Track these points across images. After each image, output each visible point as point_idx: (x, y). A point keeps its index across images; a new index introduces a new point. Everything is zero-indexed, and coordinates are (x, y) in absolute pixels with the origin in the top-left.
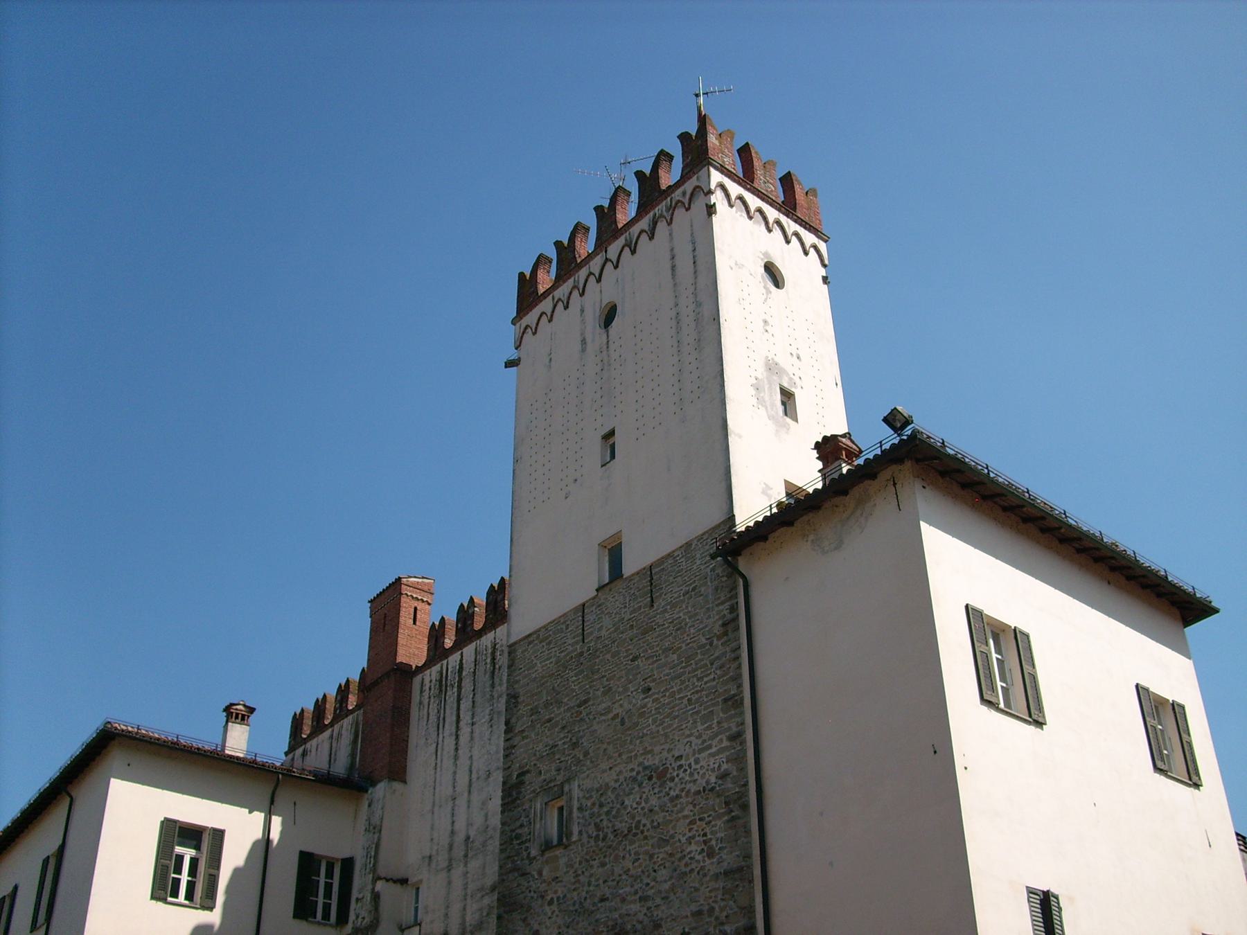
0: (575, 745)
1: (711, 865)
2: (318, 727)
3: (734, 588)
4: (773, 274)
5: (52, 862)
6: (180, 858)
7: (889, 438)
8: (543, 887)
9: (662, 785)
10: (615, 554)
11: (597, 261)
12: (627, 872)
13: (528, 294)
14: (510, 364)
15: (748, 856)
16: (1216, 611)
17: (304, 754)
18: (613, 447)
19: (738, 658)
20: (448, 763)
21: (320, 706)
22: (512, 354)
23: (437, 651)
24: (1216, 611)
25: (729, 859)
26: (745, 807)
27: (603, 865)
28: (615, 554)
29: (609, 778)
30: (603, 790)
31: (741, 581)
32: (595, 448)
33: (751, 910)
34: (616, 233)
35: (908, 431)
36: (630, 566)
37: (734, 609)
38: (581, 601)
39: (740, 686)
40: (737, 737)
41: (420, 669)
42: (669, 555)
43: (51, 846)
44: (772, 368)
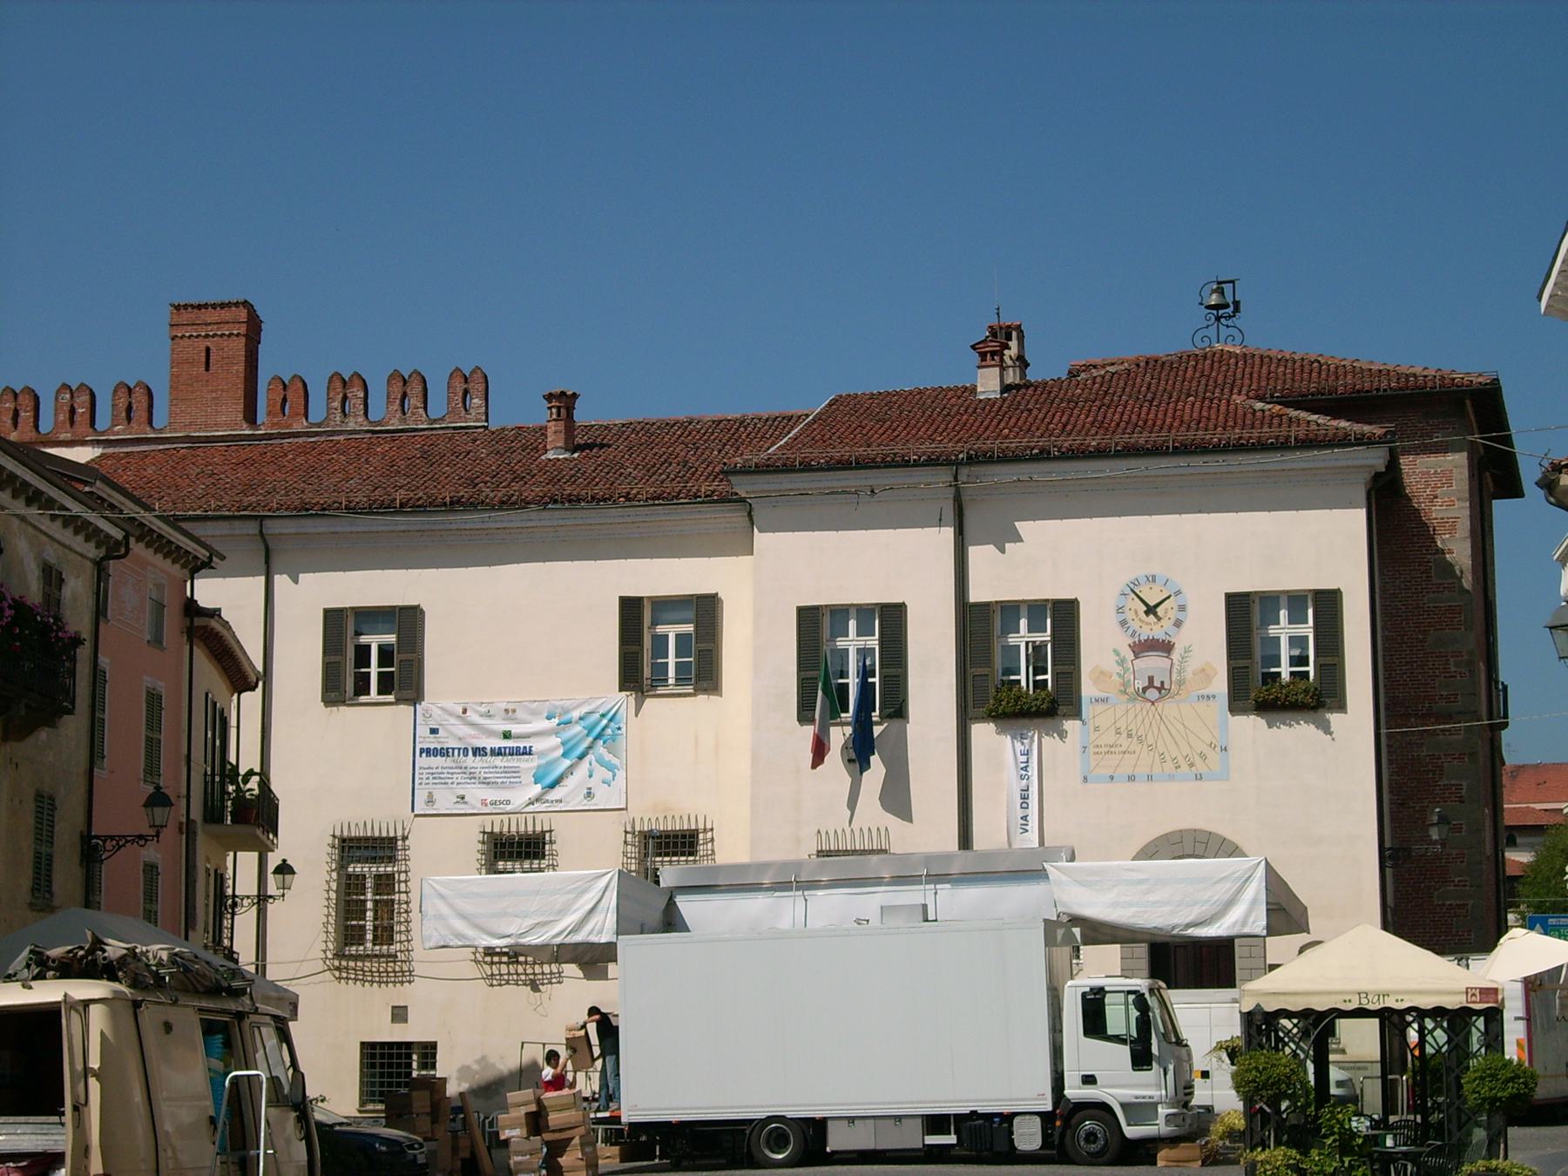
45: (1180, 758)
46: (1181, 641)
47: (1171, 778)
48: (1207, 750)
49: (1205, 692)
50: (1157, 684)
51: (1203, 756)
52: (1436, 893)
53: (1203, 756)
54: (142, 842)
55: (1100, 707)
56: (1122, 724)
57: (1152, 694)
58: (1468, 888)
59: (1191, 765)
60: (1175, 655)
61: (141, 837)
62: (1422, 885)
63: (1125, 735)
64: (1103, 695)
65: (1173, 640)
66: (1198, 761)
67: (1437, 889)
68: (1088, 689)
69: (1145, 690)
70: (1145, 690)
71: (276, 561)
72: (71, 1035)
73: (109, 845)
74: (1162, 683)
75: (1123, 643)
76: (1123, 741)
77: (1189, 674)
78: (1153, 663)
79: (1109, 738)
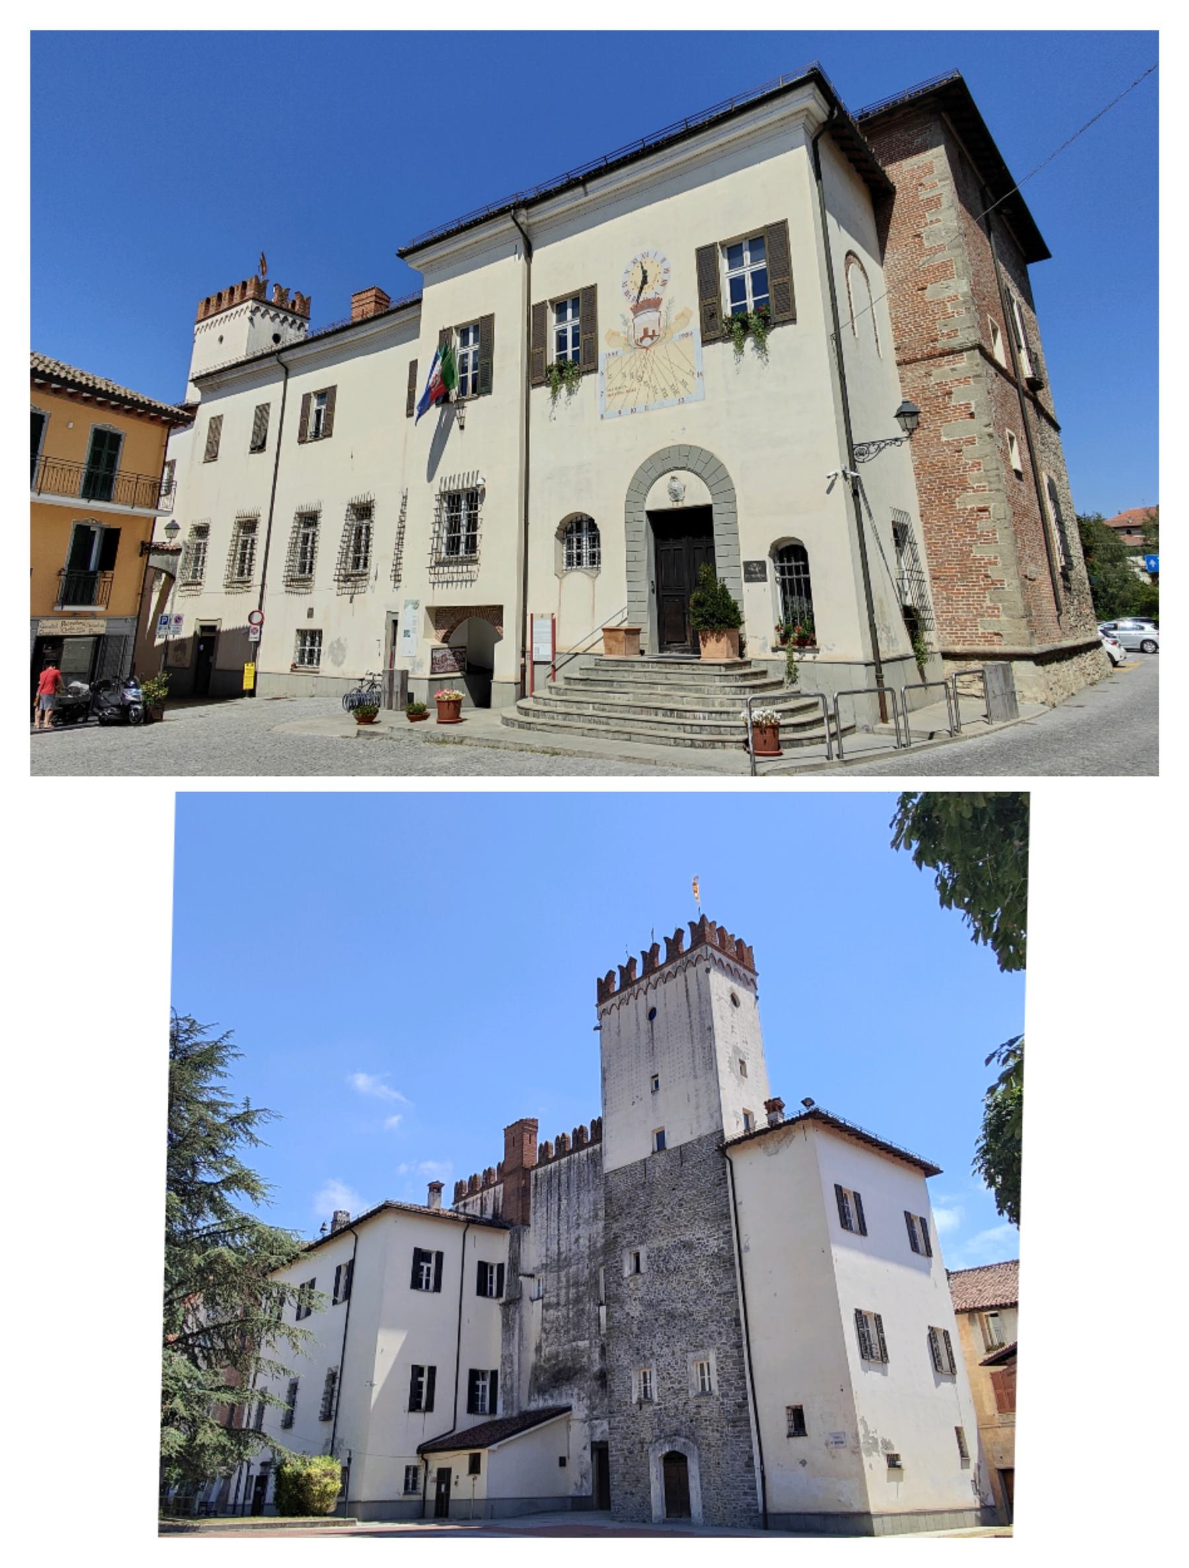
0: (644, 1226)
1: (717, 1290)
2: (472, 1192)
3: (724, 1164)
4: (735, 1001)
5: (344, 1271)
6: (423, 1267)
7: (804, 1110)
8: (630, 1292)
9: (691, 1251)
10: (660, 1137)
11: (644, 983)
12: (674, 1289)
13: (604, 991)
14: (596, 1029)
15: (736, 1287)
16: (942, 1172)
17: (465, 1205)
18: (657, 1083)
19: (727, 1196)
20: (554, 1218)
21: (473, 1179)
22: (597, 1023)
23: (545, 1158)
24: (942, 1172)
25: (727, 1287)
26: (733, 1265)
27: (662, 1284)
28: (660, 1137)
29: (664, 1244)
30: (660, 1250)
31: (728, 1162)
32: (648, 1086)
33: (738, 1311)
34: (655, 970)
35: (813, 1107)
36: (671, 1144)
37: (724, 1173)
38: (643, 1157)
39: (729, 1209)
40: (728, 1232)
41: (533, 1168)
42: (690, 1143)
43: (345, 1260)
44: (736, 1050)
45: (668, 389)
46: (666, 295)
47: (662, 406)
48: (688, 379)
49: (684, 331)
50: (650, 333)
51: (684, 383)
52: (957, 499)
53: (684, 383)
54: (899, 443)
55: (612, 360)
56: (627, 370)
57: (647, 342)
58: (987, 492)
59: (676, 392)
60: (662, 308)
61: (896, 440)
62: (944, 493)
63: (628, 378)
64: (615, 351)
65: (660, 296)
66: (680, 387)
67: (958, 496)
68: (603, 348)
69: (642, 339)
70: (642, 339)
71: (290, 373)
72: (1070, 658)
73: (872, 449)
74: (654, 331)
75: (627, 305)
76: (628, 382)
77: (672, 319)
78: (648, 319)
79: (618, 382)
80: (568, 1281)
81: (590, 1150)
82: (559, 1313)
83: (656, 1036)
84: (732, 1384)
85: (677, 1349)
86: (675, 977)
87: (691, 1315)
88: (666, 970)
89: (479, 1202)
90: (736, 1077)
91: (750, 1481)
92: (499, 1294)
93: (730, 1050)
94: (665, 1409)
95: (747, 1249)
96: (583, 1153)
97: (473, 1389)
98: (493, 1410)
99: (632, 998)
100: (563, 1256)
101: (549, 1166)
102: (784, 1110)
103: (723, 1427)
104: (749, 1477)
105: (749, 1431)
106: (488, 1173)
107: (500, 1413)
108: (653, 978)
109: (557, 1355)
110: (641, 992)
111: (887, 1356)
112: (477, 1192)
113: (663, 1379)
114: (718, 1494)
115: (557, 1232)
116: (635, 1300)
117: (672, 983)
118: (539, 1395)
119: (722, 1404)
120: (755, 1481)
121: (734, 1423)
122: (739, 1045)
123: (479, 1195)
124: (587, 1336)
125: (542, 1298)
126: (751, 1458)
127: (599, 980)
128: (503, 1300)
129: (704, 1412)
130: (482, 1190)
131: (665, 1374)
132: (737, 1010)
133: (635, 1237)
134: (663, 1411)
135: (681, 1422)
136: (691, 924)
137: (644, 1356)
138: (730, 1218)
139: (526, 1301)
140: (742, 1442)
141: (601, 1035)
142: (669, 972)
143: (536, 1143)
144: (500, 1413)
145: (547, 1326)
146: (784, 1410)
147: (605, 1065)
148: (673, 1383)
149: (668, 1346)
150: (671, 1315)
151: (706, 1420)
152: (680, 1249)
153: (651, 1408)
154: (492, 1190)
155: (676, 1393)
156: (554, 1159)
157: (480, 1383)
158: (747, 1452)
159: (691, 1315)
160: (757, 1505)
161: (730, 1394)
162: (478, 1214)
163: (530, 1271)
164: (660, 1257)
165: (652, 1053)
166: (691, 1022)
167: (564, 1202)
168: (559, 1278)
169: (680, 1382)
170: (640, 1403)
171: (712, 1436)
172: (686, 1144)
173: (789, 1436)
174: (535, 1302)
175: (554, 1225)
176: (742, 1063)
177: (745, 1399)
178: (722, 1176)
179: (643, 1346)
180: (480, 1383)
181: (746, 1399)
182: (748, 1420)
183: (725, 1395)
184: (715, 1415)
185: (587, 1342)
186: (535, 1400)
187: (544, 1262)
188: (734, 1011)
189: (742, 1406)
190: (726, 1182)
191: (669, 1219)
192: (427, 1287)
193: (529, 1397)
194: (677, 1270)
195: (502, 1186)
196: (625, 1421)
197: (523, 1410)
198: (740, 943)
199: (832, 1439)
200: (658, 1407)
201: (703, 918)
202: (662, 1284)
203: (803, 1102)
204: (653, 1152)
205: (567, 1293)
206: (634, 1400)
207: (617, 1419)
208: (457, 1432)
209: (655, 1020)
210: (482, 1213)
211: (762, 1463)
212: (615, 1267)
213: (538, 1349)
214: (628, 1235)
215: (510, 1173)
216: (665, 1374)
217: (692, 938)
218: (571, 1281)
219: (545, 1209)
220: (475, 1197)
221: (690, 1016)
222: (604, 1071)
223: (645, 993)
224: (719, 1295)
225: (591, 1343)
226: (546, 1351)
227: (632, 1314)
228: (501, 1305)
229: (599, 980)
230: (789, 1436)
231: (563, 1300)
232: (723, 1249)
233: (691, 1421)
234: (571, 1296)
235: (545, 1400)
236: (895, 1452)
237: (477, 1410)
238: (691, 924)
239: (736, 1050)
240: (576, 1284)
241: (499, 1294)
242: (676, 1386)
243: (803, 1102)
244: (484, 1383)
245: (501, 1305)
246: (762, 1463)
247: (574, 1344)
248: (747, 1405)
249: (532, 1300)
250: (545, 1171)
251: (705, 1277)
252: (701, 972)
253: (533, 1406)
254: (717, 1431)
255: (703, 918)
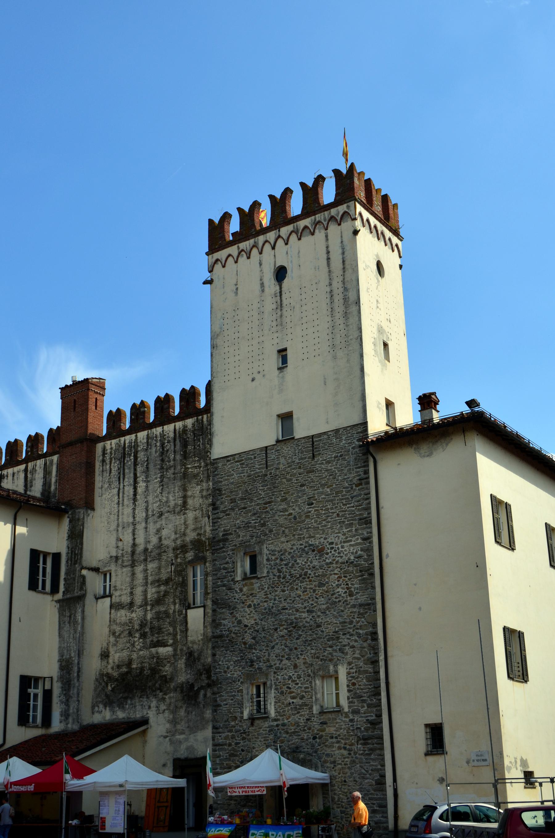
14: (206, 282)
19: (369, 498)
22: (207, 276)
25: (362, 598)
26: (372, 575)
27: (283, 591)
30: (283, 552)
32: (274, 361)
33: (375, 625)
39: (370, 513)
42: (325, 433)
44: (381, 330)
80: (146, 578)
81: (179, 425)
82: (134, 615)
83: (285, 302)
84: (364, 701)
85: (300, 662)
86: (313, 234)
87: (319, 626)
88: (302, 224)
89: (22, 475)
90: (380, 361)
91: (380, 799)
92: (55, 589)
93: (375, 330)
94: (284, 725)
95: (387, 556)
96: (169, 428)
97: (24, 697)
98: (47, 721)
99: (255, 252)
100: (140, 548)
101: (122, 439)
102: (438, 407)
103: (352, 745)
104: (380, 795)
105: (382, 749)
106: (34, 440)
107: (57, 726)
108: (285, 231)
109: (130, 662)
110: (267, 247)
111: (527, 675)
112: (19, 463)
113: (282, 693)
114: (342, 812)
115: (131, 520)
116: (250, 606)
117: (307, 239)
118: (105, 707)
119: (352, 721)
120: (385, 799)
121: (365, 740)
122: (383, 324)
123: (23, 467)
124: (171, 642)
125: (110, 596)
126: (383, 776)
127: (211, 222)
128: (60, 596)
129: (331, 730)
130: (26, 461)
131: (285, 689)
132: (382, 281)
133: (252, 537)
134: (280, 727)
135: (302, 739)
136: (337, 172)
137: (260, 669)
138: (371, 523)
139: (89, 599)
140: (373, 760)
141: (212, 291)
142: (306, 227)
143: (102, 408)
144: (57, 726)
145: (118, 629)
146: (423, 728)
147: (217, 329)
148: (293, 698)
149: (288, 659)
150: (294, 626)
151: (332, 738)
152: (307, 553)
153: (266, 724)
154: (40, 463)
155: (297, 709)
156: (129, 432)
157: (32, 691)
158: (378, 770)
159: (319, 626)
160: (387, 822)
161: (363, 711)
162: (21, 489)
163: (94, 564)
164: (282, 560)
165: (280, 323)
166: (331, 291)
167: (141, 485)
168: (133, 574)
169: (302, 697)
170: (252, 720)
171: (337, 753)
172: (320, 435)
173: (427, 754)
174: (100, 601)
175: (128, 511)
176: (385, 345)
177: (380, 716)
178: (363, 476)
179: (259, 658)
180: (32, 691)
181: (380, 716)
182: (381, 738)
183: (356, 712)
184: (343, 732)
185: (170, 649)
186: (100, 712)
187: (114, 554)
188: (378, 281)
189: (376, 723)
190: (368, 483)
191: (295, 518)
192: (44, 587)
193: (93, 707)
194: (304, 576)
195: (55, 458)
196: (233, 737)
197: (85, 723)
198: (385, 199)
199: (474, 757)
200: (275, 723)
201: (352, 168)
202: (283, 591)
203: (467, 403)
204: (278, 441)
205: (145, 592)
206: (246, 715)
207: (223, 735)
208: (7, 746)
209: (286, 283)
210: (26, 491)
211: (395, 780)
212: (225, 569)
213: (105, 655)
214: (241, 534)
215: (71, 444)
216: (285, 689)
217: (337, 190)
218: (150, 579)
219: (115, 491)
220: (16, 469)
221: (330, 285)
222: (214, 337)
223: (273, 248)
224: (354, 606)
225: (175, 650)
226: (116, 656)
227: (246, 622)
228: (58, 601)
229: (211, 222)
230: (427, 754)
231: (138, 599)
232: (360, 557)
233: (314, 738)
234: (149, 596)
235: (113, 712)
236: (530, 770)
237: (28, 722)
238: (337, 172)
239: (381, 330)
240: (158, 582)
241: (55, 589)
242: (297, 701)
243: (467, 403)
244: (36, 691)
245: (58, 601)
246: (395, 780)
247: (153, 650)
248: (381, 722)
249: (97, 598)
250: (118, 445)
251: (338, 586)
252: (348, 234)
253: (97, 719)
254: (345, 748)
255: (352, 168)
